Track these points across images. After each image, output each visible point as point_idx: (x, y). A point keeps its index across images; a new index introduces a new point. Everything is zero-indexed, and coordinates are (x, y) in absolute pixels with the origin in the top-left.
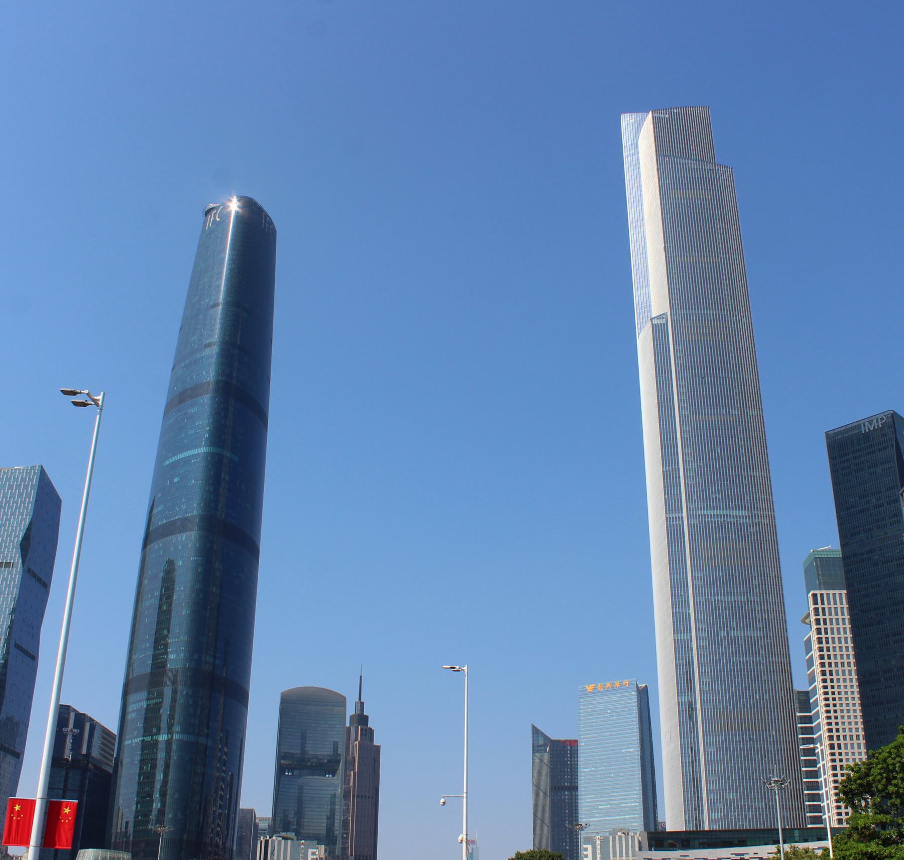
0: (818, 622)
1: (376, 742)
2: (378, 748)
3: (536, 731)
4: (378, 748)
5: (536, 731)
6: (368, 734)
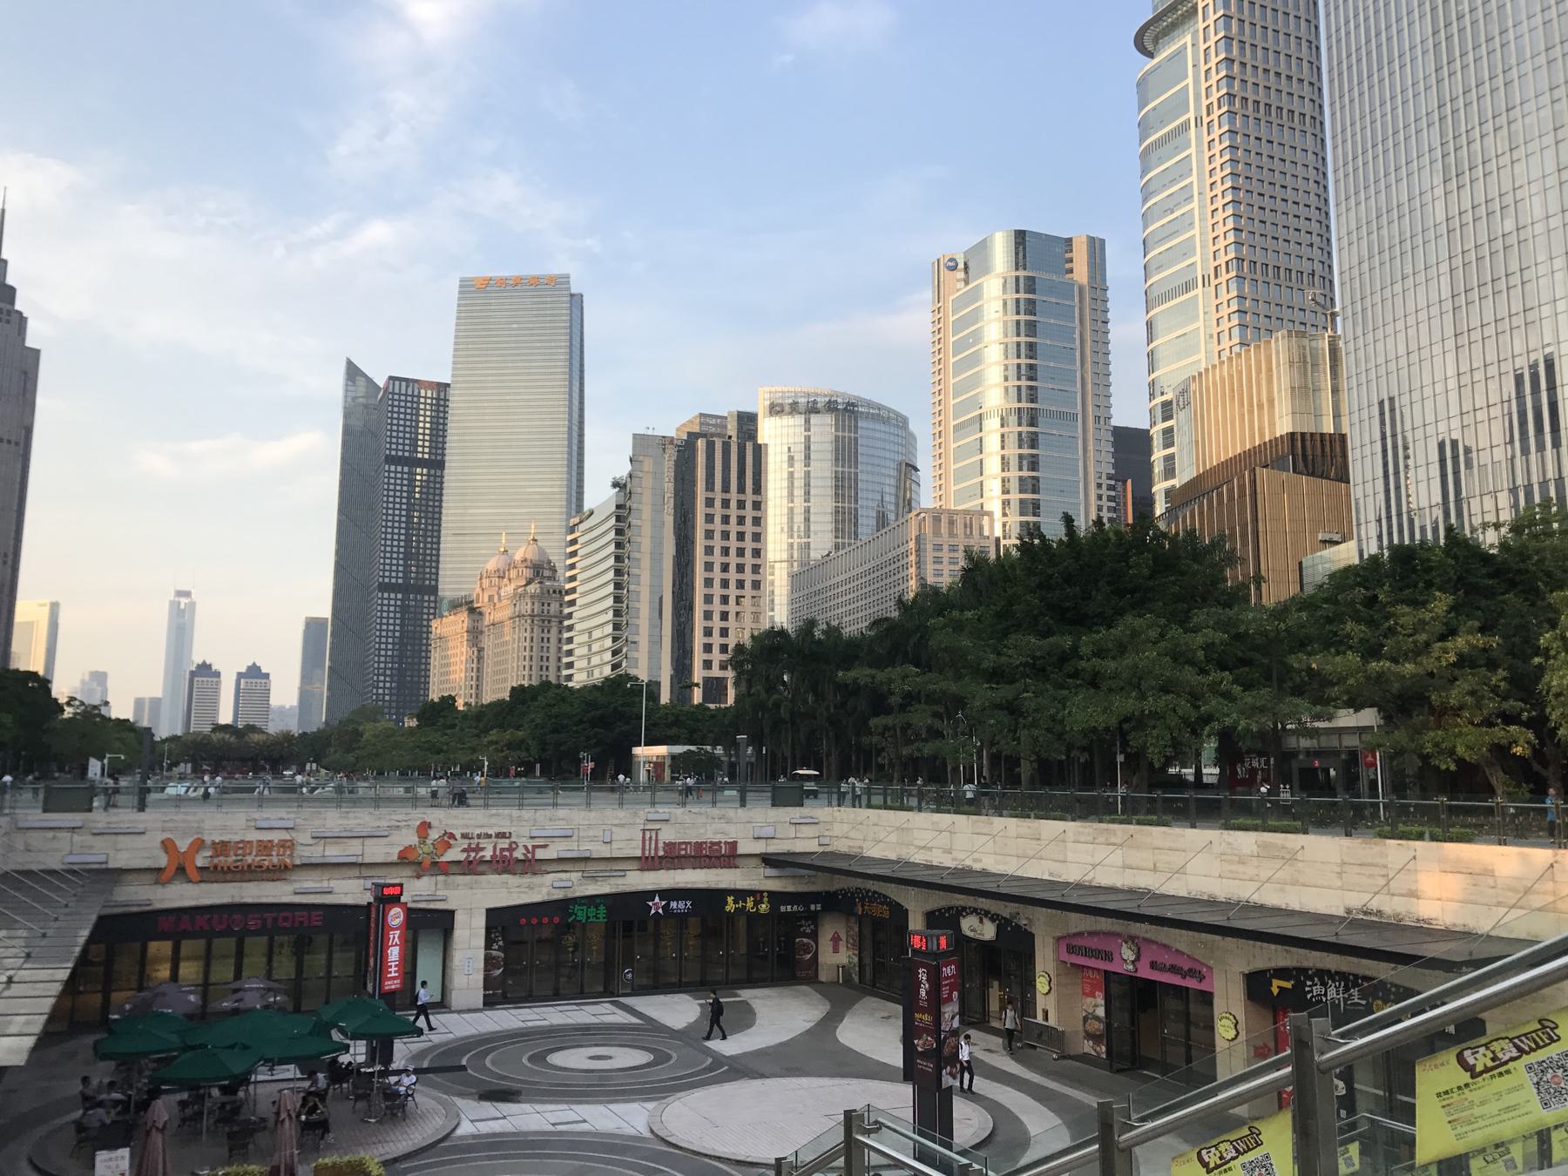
1: (30, 342)
2: (37, 353)
3: (353, 372)
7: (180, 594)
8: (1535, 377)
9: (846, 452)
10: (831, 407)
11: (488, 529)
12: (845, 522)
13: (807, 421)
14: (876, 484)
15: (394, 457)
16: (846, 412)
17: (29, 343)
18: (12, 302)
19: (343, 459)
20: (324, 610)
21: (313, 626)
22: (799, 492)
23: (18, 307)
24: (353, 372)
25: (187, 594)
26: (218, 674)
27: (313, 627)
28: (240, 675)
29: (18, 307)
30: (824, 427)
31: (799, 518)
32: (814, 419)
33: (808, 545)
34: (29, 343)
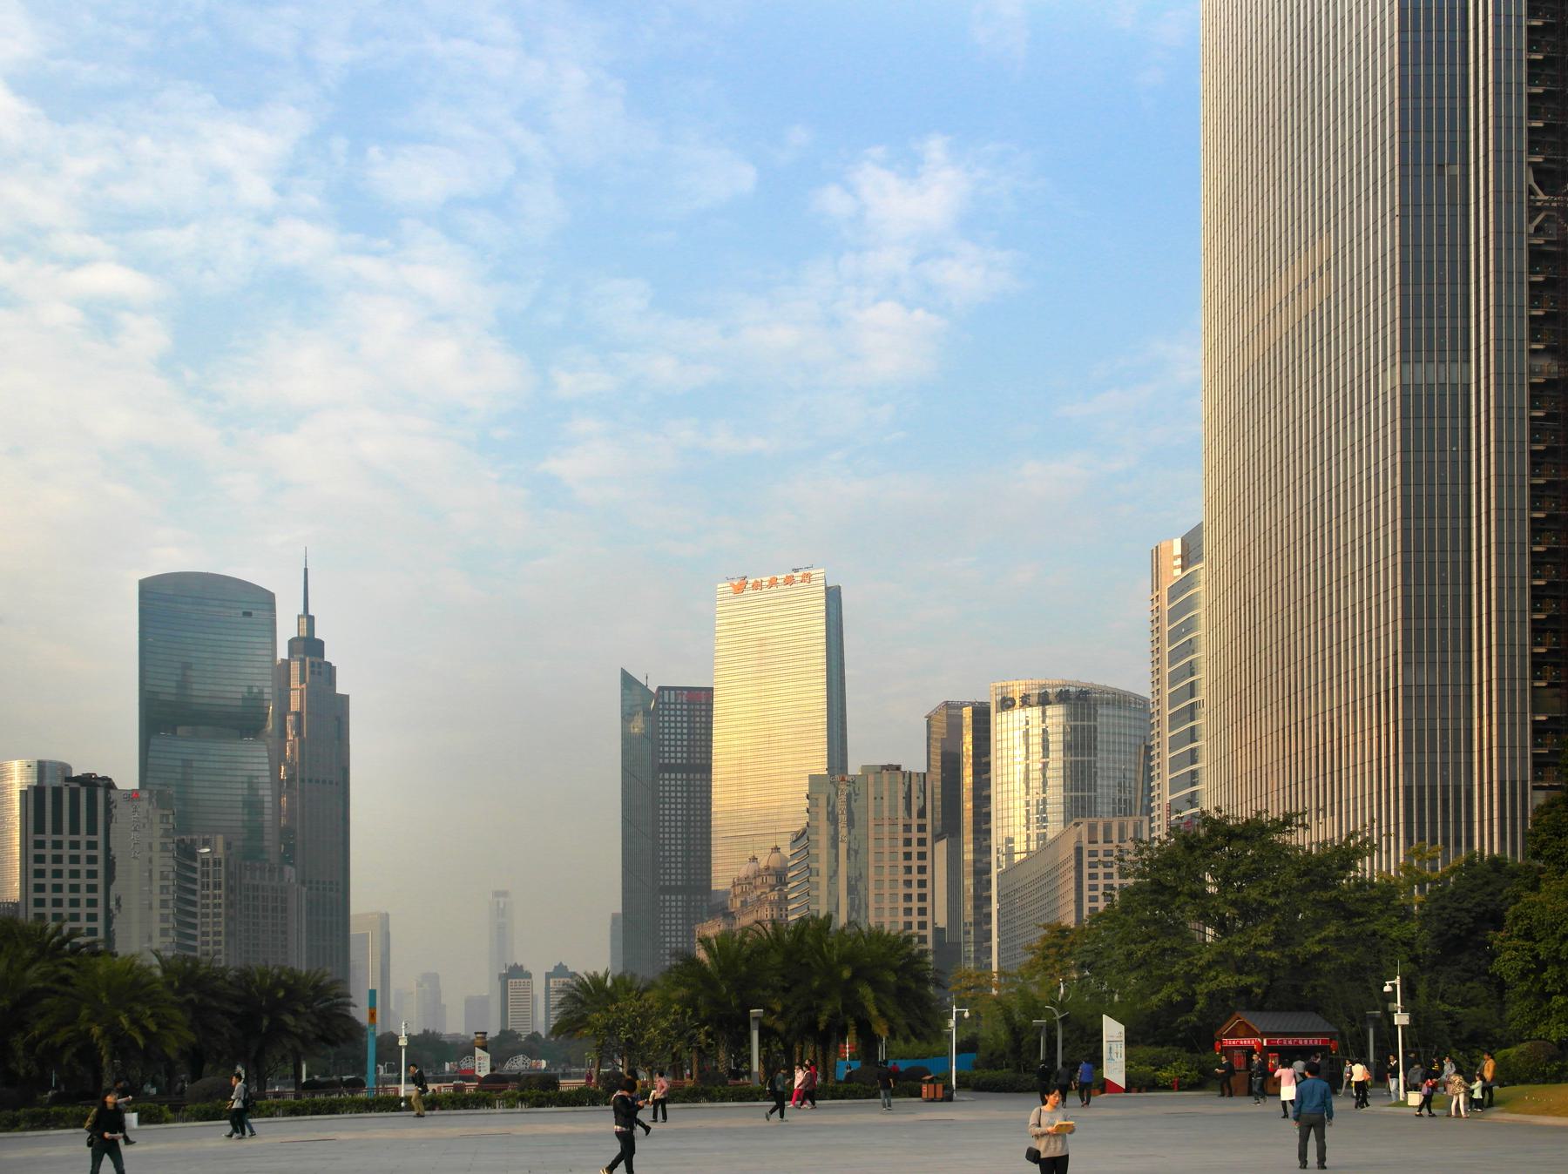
1: (340, 690)
3: (628, 681)
7: (497, 894)
8: (1430, 396)
9: (1080, 743)
10: (1063, 697)
12: (1078, 807)
13: (1044, 713)
14: (1110, 763)
16: (1080, 703)
17: (339, 691)
18: (322, 655)
19: (623, 767)
20: (619, 909)
21: (614, 917)
22: (1036, 748)
23: (326, 659)
24: (628, 681)
25: (504, 894)
26: (529, 975)
27: (614, 917)
28: (548, 976)
29: (326, 659)
30: (1056, 713)
31: (1036, 775)
32: (1050, 710)
33: (1044, 801)
34: (339, 691)
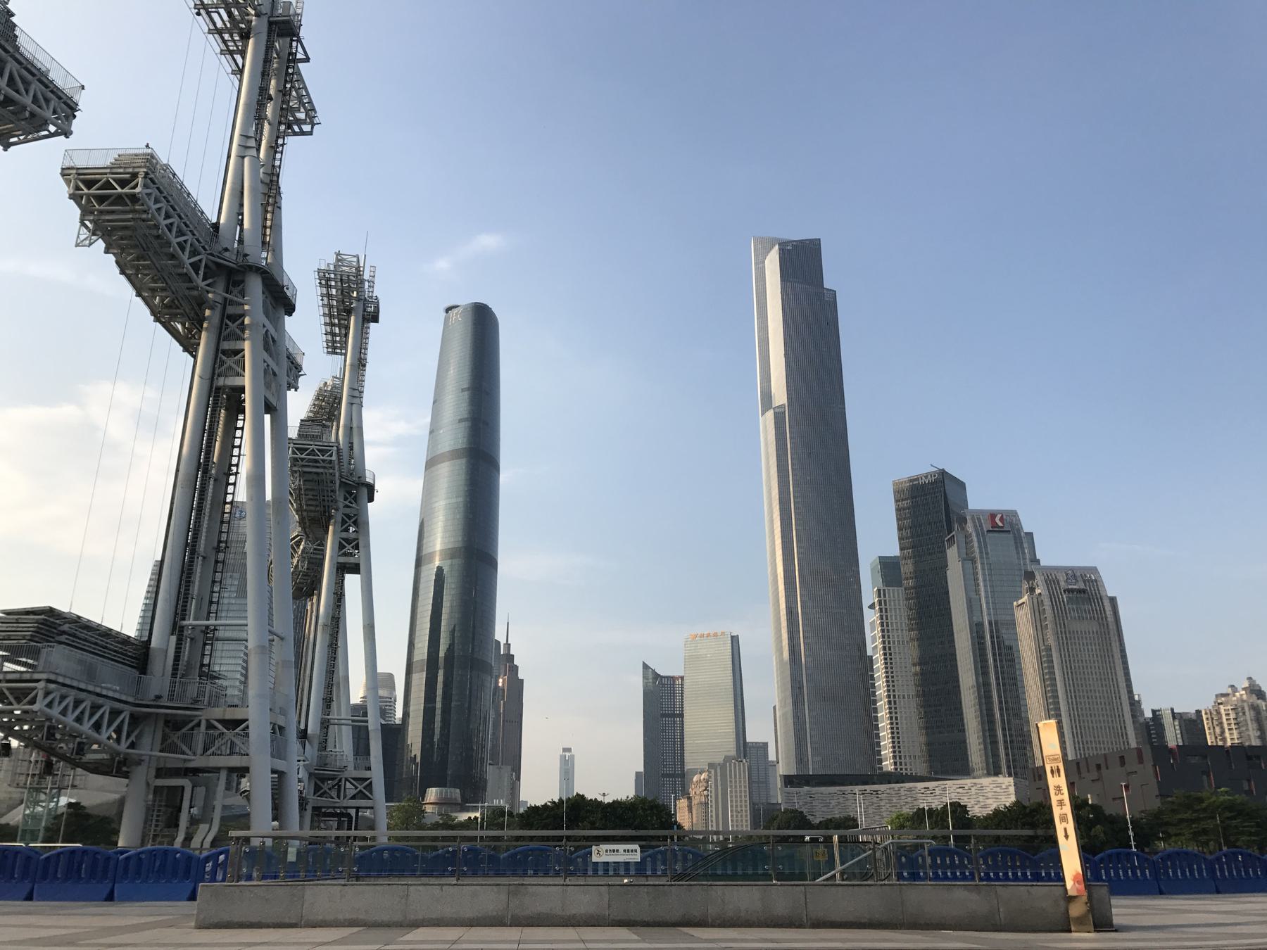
0: (881, 610)
2: (522, 681)
3: (645, 667)
4: (522, 681)
5: (645, 667)
6: (515, 669)
11: (706, 733)
15: (662, 704)
